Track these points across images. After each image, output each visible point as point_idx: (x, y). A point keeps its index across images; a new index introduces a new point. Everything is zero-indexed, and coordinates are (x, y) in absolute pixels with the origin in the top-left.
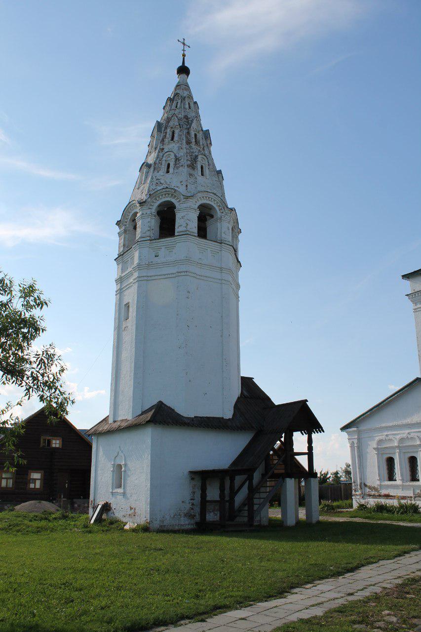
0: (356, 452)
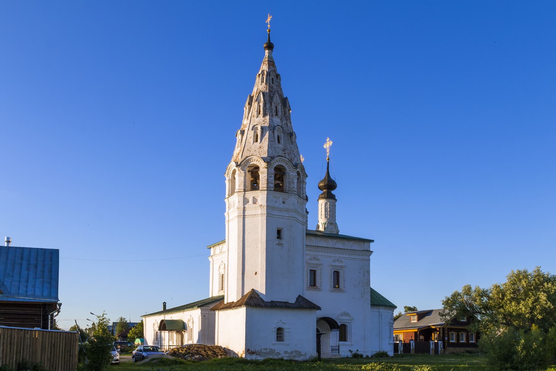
0: (464, 338)
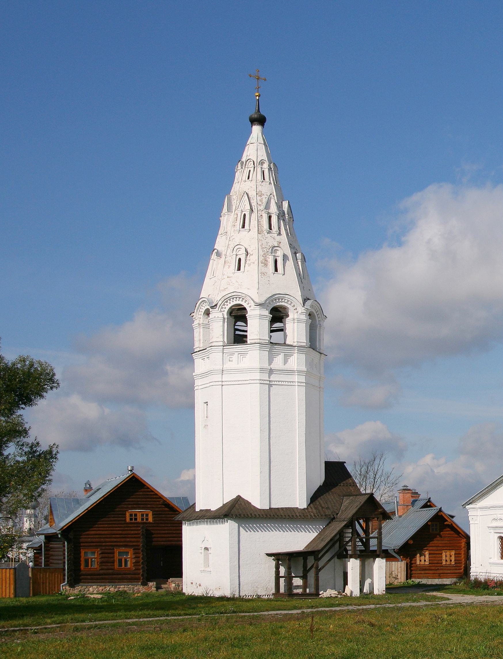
0: (297, 406)
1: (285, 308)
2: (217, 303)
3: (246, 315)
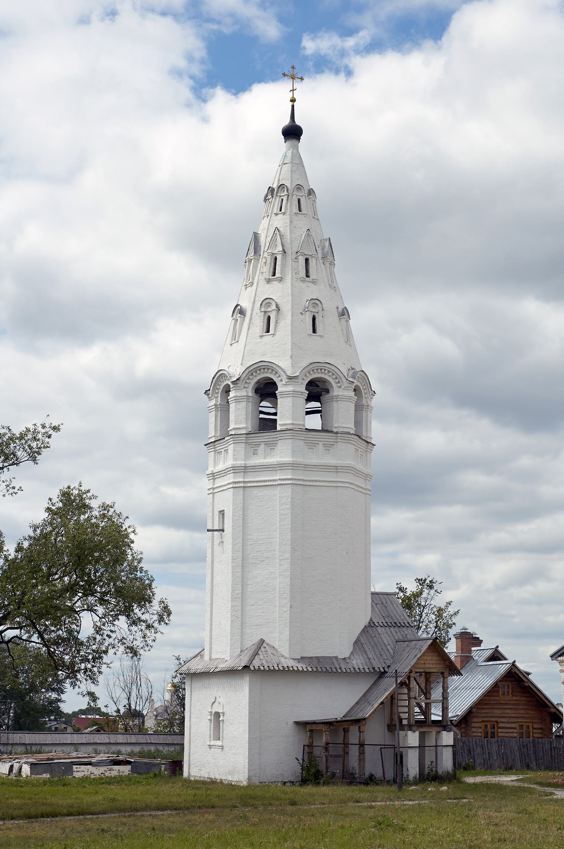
1: (324, 381)
2: (239, 376)
3: (277, 392)
